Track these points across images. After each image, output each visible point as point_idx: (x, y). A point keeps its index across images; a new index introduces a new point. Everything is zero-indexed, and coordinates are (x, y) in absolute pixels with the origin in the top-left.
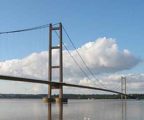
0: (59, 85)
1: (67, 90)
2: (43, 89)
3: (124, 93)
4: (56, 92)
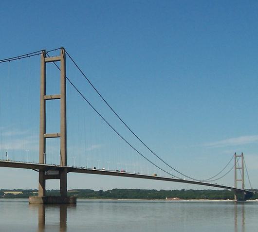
0: (61, 172)
1: (75, 182)
2: (30, 180)
3: (240, 187)
4: (53, 185)
